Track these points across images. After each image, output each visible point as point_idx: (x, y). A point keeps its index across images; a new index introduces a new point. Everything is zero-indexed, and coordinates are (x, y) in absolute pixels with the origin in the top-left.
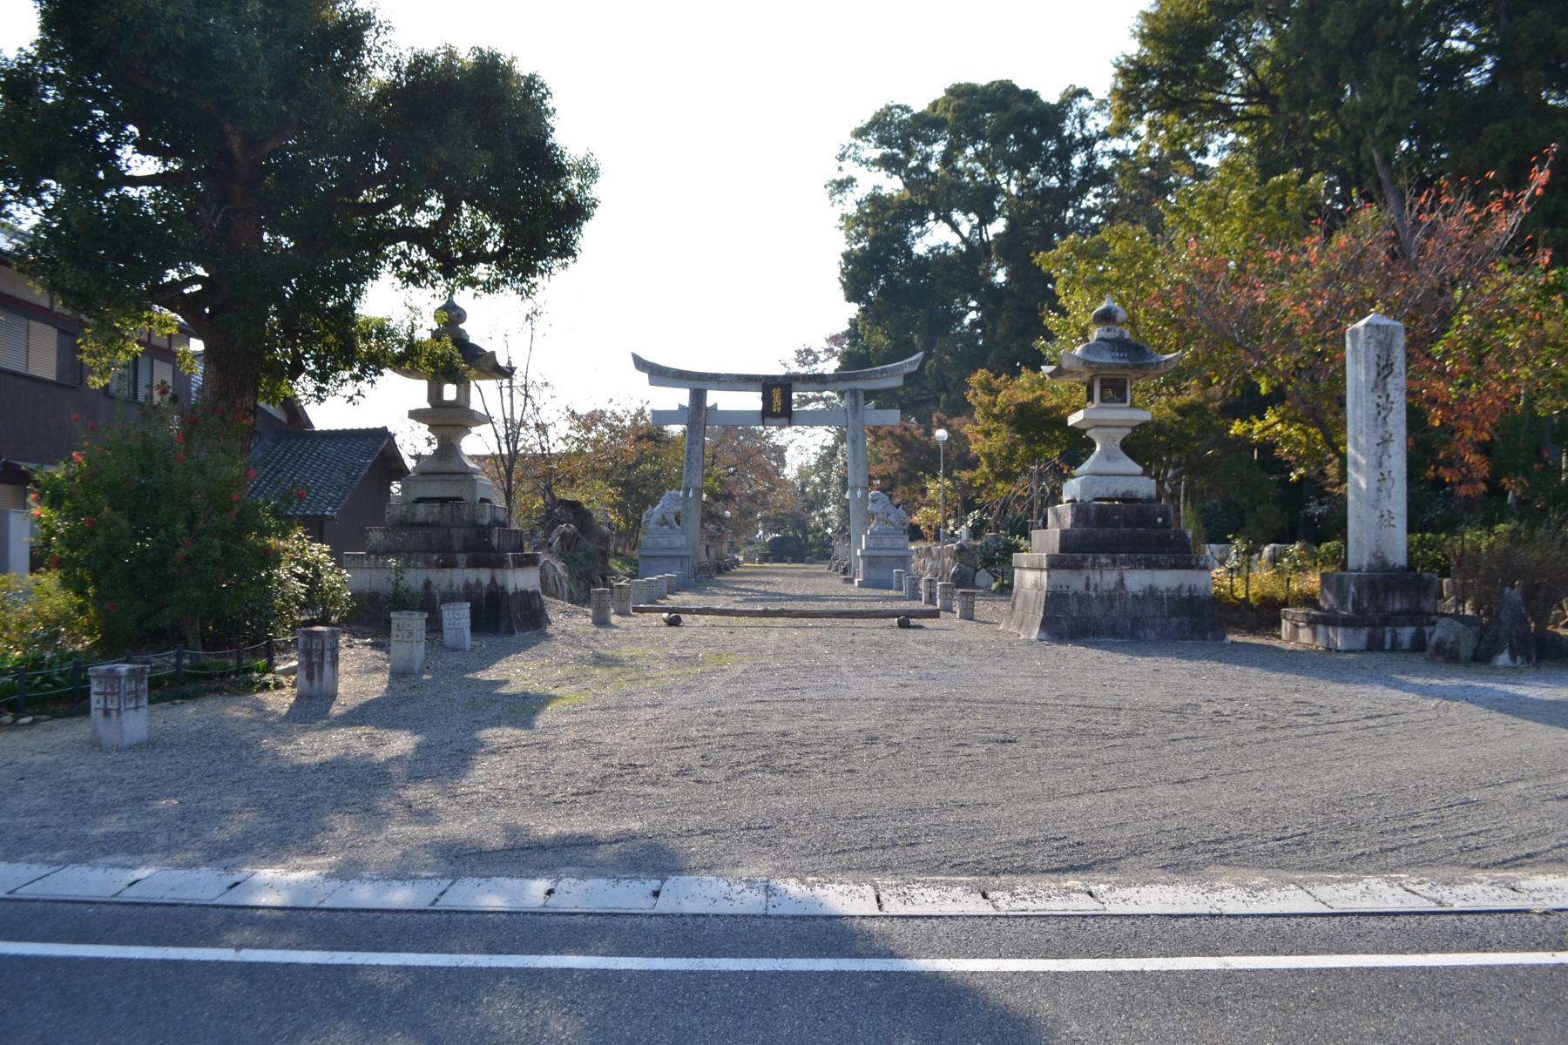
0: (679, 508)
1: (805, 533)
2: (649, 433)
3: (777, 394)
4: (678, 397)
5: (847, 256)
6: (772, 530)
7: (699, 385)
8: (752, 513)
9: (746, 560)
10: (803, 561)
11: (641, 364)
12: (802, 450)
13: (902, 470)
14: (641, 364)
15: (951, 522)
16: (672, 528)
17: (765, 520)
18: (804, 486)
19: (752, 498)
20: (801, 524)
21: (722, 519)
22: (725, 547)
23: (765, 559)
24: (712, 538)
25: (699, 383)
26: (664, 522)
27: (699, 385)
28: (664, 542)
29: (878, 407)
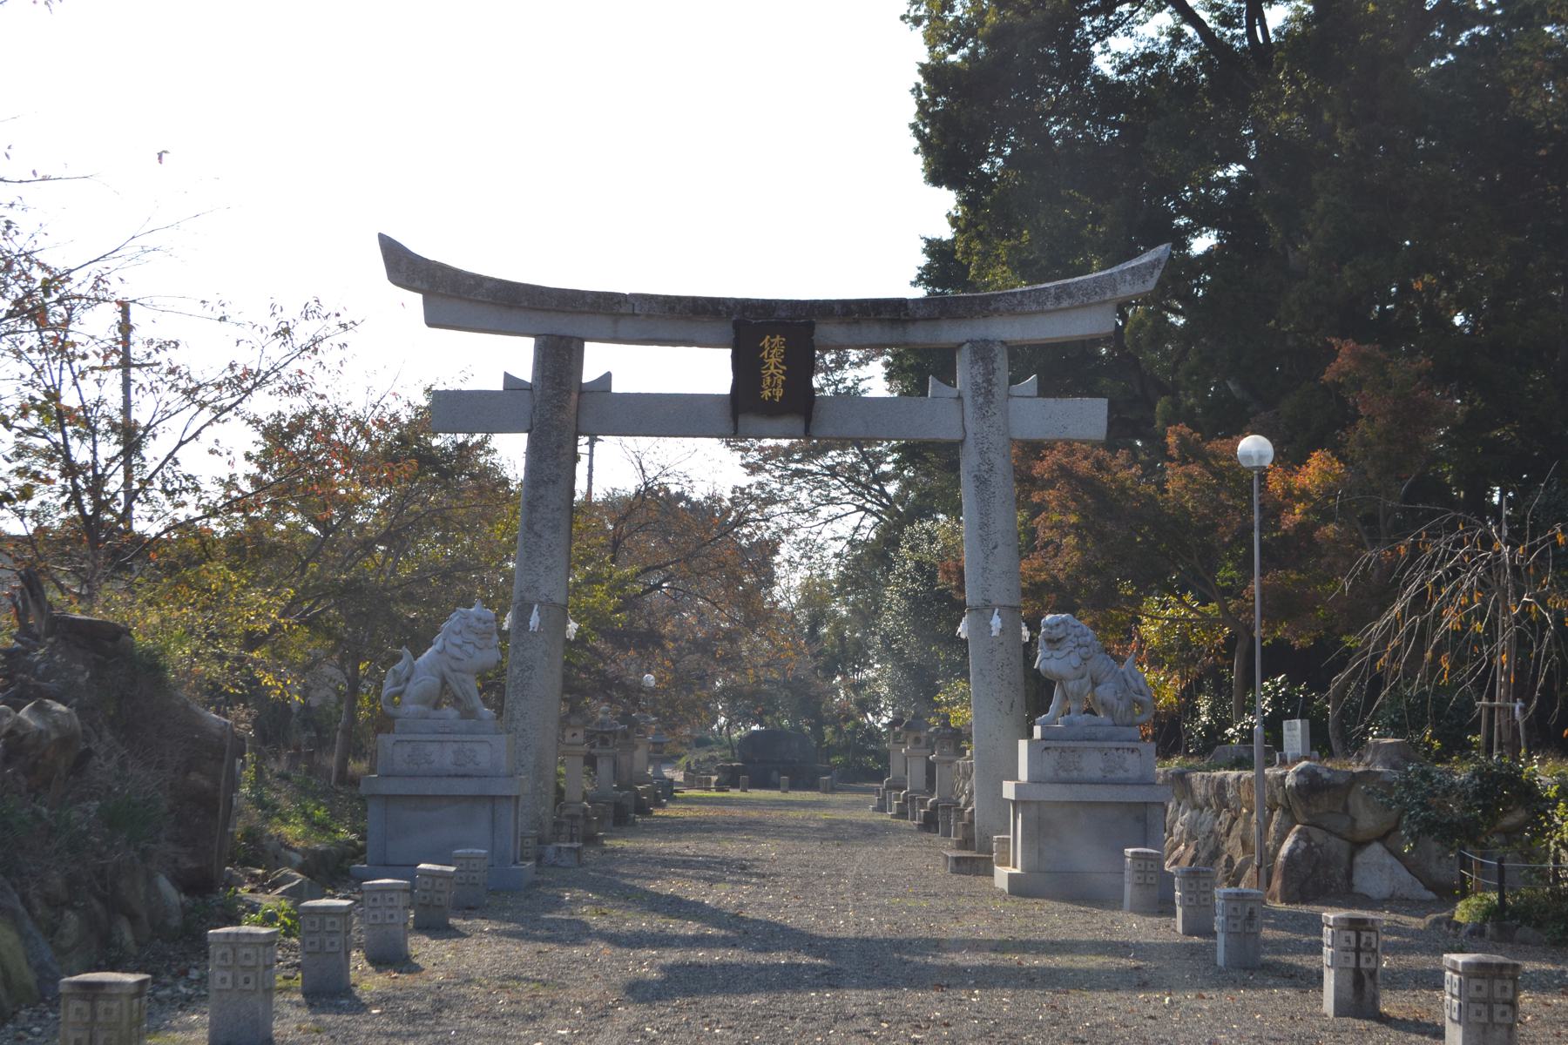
0: (490, 656)
1: (818, 724)
2: (421, 454)
3: (773, 352)
4: (504, 358)
5: (934, 74)
6: (747, 717)
7: (562, 325)
8: (704, 679)
9: (691, 782)
10: (812, 786)
11: (403, 266)
12: (809, 548)
13: (1088, 569)
14: (403, 266)
15: (1204, 704)
16: (468, 714)
17: (732, 694)
18: (815, 622)
19: (703, 647)
20: (810, 704)
21: (634, 692)
22: (641, 754)
23: (731, 779)
24: (600, 737)
25: (561, 320)
26: (445, 692)
27: (562, 325)
28: (443, 756)
29: (1044, 391)
